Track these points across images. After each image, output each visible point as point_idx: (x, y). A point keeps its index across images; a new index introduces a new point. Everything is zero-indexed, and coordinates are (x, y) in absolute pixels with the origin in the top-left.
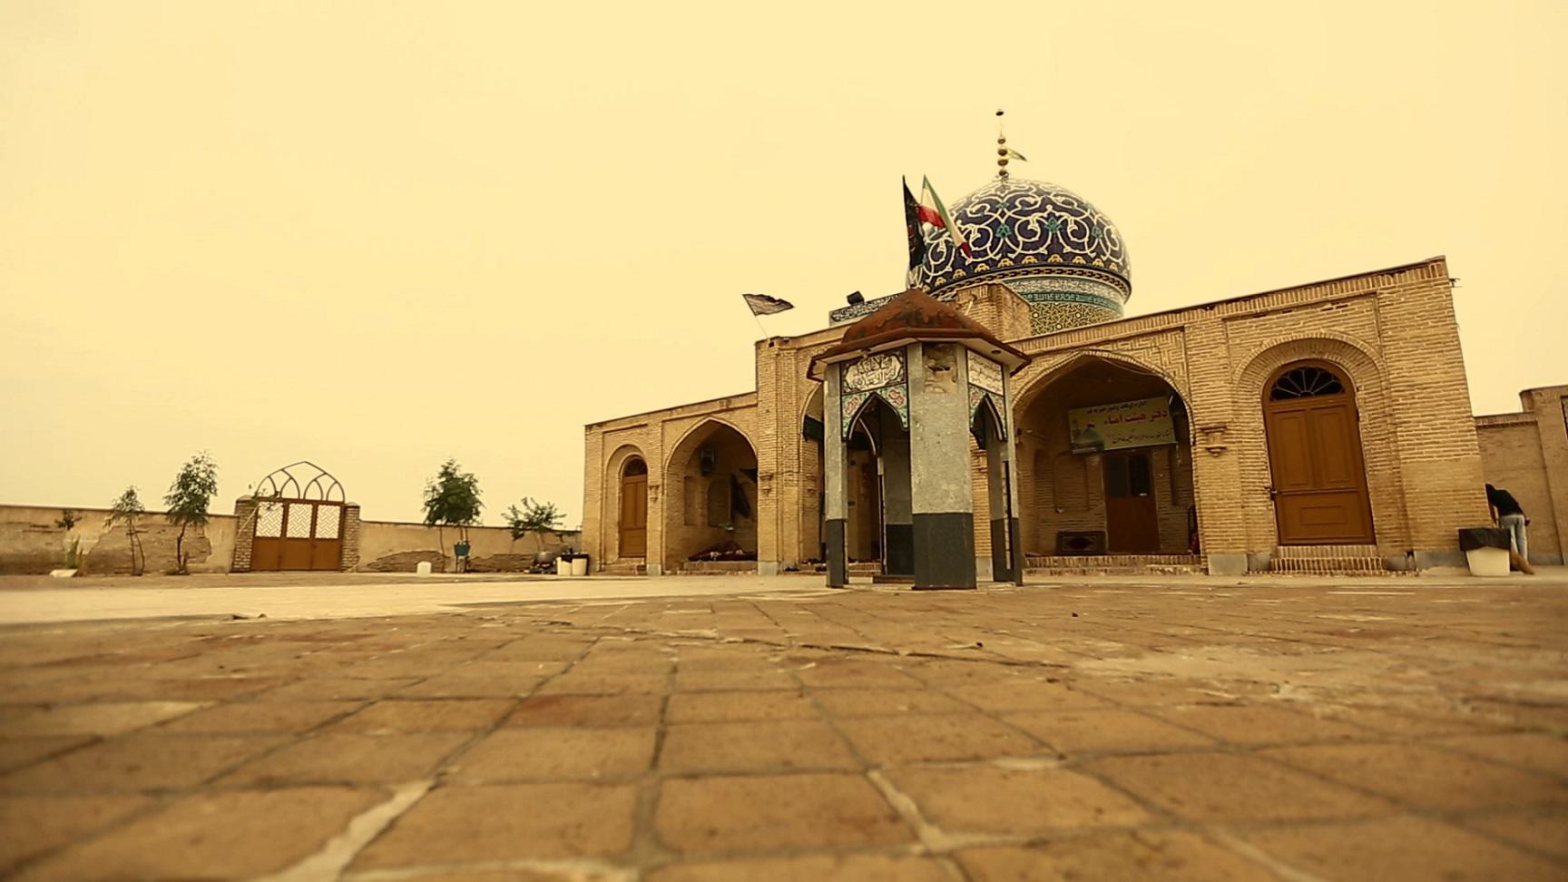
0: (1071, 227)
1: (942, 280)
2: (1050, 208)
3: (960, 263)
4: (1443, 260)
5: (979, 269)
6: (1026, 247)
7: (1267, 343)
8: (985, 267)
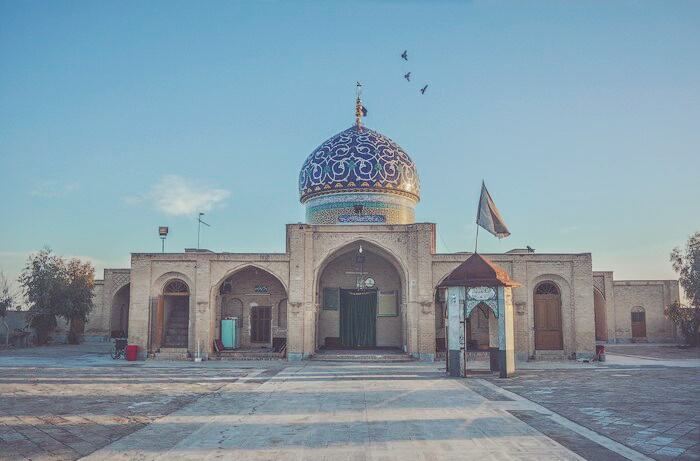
0: (362, 165)
1: (318, 189)
2: (352, 154)
3: (352, 178)
4: (433, 226)
5: (363, 184)
6: (389, 178)
7: (540, 273)
8: (367, 185)
